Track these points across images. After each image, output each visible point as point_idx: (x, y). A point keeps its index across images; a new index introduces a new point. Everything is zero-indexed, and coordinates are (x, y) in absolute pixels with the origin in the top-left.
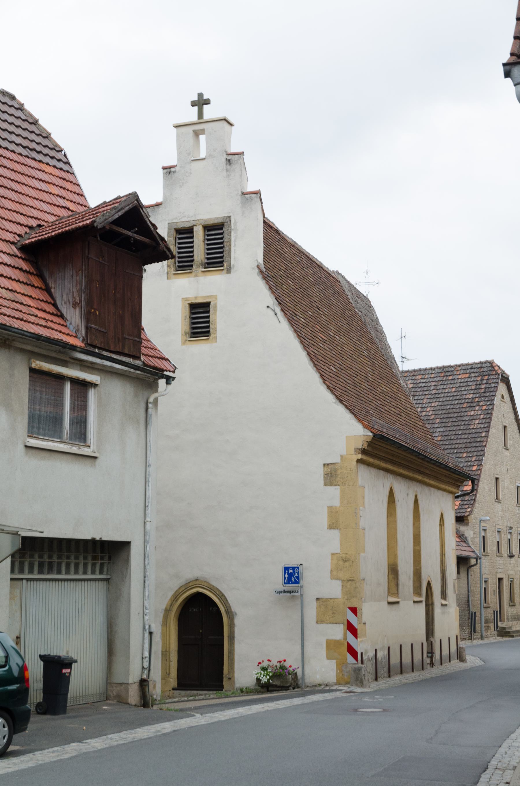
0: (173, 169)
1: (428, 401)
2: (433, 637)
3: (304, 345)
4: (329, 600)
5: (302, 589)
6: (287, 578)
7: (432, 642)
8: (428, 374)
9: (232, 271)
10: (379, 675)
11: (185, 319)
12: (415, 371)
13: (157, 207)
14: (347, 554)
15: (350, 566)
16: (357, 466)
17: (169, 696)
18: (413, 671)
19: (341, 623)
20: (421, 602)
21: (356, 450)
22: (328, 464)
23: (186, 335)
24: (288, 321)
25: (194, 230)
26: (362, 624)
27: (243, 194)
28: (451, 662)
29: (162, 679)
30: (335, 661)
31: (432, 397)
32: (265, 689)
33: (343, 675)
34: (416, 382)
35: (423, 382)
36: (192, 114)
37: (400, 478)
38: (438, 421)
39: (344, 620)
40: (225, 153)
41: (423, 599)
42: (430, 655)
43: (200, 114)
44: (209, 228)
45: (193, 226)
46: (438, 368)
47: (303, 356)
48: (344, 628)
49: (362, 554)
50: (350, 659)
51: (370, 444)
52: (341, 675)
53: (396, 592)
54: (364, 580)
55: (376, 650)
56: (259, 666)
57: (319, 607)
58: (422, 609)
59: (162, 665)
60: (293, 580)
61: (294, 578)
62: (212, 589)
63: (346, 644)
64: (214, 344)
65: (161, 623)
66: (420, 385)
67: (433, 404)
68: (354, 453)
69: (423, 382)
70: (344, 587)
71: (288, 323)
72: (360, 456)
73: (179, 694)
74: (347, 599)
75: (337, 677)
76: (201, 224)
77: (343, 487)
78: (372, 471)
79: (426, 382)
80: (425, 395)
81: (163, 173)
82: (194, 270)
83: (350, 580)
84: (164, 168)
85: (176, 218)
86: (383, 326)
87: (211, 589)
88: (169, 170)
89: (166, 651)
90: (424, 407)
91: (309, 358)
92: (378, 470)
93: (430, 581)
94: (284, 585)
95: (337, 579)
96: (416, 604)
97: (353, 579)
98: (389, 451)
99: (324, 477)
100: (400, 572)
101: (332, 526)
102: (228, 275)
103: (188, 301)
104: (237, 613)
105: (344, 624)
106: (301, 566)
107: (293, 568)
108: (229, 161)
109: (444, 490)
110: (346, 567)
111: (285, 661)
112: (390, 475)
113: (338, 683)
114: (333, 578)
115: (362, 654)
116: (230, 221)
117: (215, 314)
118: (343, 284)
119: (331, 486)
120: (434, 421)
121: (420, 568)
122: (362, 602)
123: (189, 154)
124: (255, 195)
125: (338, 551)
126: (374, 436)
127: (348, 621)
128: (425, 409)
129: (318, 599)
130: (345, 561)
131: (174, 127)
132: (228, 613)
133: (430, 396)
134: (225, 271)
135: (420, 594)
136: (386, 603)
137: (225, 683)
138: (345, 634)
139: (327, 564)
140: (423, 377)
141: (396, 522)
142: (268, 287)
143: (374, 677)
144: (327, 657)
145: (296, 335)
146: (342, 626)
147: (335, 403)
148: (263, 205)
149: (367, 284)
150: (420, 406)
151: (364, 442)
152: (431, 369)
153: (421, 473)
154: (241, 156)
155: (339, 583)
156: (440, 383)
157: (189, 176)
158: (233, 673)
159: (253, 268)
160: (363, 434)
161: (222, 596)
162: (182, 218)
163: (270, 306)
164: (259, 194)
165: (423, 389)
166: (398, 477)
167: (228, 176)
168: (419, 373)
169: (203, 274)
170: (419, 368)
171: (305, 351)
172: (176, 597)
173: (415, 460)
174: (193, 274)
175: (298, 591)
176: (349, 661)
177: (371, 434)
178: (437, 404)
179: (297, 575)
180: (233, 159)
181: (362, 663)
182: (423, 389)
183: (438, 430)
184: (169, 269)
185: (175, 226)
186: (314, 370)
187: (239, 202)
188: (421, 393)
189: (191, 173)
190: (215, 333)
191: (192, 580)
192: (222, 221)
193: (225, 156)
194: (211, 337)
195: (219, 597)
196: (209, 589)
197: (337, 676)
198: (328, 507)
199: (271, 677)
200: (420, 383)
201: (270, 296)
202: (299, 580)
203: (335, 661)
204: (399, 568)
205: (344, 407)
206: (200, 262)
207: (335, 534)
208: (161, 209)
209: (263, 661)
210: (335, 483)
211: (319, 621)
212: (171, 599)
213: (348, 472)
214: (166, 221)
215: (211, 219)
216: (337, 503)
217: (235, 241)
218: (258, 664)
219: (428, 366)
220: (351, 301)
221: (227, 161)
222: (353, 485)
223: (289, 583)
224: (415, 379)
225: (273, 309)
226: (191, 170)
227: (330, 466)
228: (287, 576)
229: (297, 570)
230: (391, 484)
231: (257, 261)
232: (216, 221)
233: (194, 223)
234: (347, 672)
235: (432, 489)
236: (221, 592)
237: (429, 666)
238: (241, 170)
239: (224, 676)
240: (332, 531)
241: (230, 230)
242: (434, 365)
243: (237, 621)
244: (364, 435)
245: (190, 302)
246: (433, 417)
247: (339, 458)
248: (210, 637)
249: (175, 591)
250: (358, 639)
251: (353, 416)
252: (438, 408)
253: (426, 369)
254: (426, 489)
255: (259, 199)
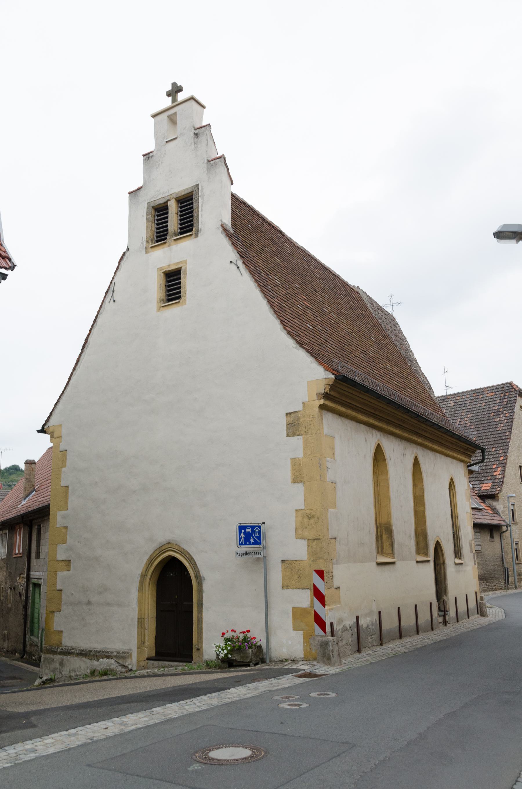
0: (151, 155)
1: (465, 413)
2: (446, 596)
3: (264, 293)
4: (295, 562)
5: (264, 550)
6: (243, 539)
7: (444, 601)
8: (465, 395)
9: (200, 234)
10: (362, 644)
11: (160, 288)
12: (455, 394)
13: (138, 191)
14: (312, 509)
15: (316, 523)
16: (321, 415)
17: (144, 666)
18: (418, 633)
19: (308, 589)
20: (428, 561)
21: (318, 395)
22: (290, 413)
23: (160, 302)
24: (249, 272)
25: (169, 204)
26: (333, 589)
27: (208, 161)
28: (470, 618)
29: (138, 648)
30: (302, 632)
31: (468, 411)
32: (226, 665)
33: (310, 649)
34: (456, 401)
35: (461, 401)
36: (168, 102)
37: (392, 438)
38: (473, 427)
39: (311, 584)
40: (193, 128)
41: (431, 558)
42: (442, 613)
43: (174, 100)
44: (181, 201)
45: (167, 202)
46: (471, 391)
47: (263, 304)
48: (310, 594)
49: (331, 510)
50: (318, 630)
51: (332, 387)
52: (308, 649)
53: (391, 552)
54: (335, 539)
55: (357, 618)
56: (223, 636)
57: (284, 570)
58: (429, 569)
59: (138, 633)
60: (252, 540)
61: (253, 538)
62: (183, 552)
63: (313, 612)
64: (184, 306)
65: (138, 588)
66: (459, 403)
67: (469, 416)
68: (316, 398)
69: (461, 401)
70: (310, 547)
71: (249, 273)
72: (322, 402)
73: (153, 665)
74: (313, 561)
75: (304, 652)
76: (174, 197)
77: (305, 436)
78: (343, 419)
79: (463, 401)
80: (463, 410)
81: (144, 160)
82: (168, 241)
83: (316, 539)
84: (144, 156)
85: (153, 197)
86: (406, 337)
87: (181, 552)
88: (148, 156)
89: (141, 618)
90: (463, 418)
91: (269, 306)
92: (358, 424)
93: (440, 541)
94: (239, 546)
95: (302, 538)
96: (420, 565)
97: (319, 537)
98: (364, 401)
99: (287, 427)
100: (395, 532)
101: (295, 481)
102: (196, 239)
103: (163, 270)
104: (205, 578)
105: (310, 590)
106: (263, 525)
107: (253, 527)
108: (196, 135)
109: (453, 458)
110: (311, 525)
111: (248, 631)
112: (376, 431)
113: (306, 659)
114: (299, 537)
115: (332, 624)
116: (198, 188)
117: (185, 278)
118: (362, 296)
119: (294, 436)
120: (470, 427)
121: (426, 528)
122: (333, 564)
123: (164, 137)
124: (219, 160)
125: (303, 507)
126: (336, 378)
127: (315, 586)
128: (463, 420)
129: (283, 561)
130: (310, 517)
131: (231, 194)
132: (197, 578)
133: (466, 410)
134: (194, 236)
135: (426, 554)
136: (415, 562)
137: (195, 654)
138: (312, 601)
139: (292, 522)
140: (461, 397)
141: (388, 480)
142: (230, 243)
143: (356, 649)
144: (293, 627)
145: (257, 285)
146: (308, 591)
147: (295, 348)
148: (229, 171)
149: (392, 305)
150: (460, 417)
151: (326, 385)
152: (467, 392)
153: (420, 436)
154: (208, 128)
155: (304, 543)
156: (474, 400)
157: (164, 157)
158: (202, 643)
159: (218, 228)
160: (325, 377)
161: (191, 560)
162: (158, 196)
163: (233, 261)
164: (222, 159)
165: (461, 406)
166: (389, 436)
167: (196, 148)
168: (458, 395)
169: (175, 242)
170: (458, 392)
171: (266, 299)
172: (150, 562)
173: (408, 420)
174: (167, 244)
175: (260, 553)
176: (316, 633)
177: (333, 377)
178: (471, 415)
179: (257, 535)
180: (200, 132)
181: (333, 635)
182: (461, 406)
183: (474, 433)
184: (147, 244)
185: (152, 205)
186: (274, 317)
187: (205, 169)
188: (460, 409)
189: (165, 154)
190: (185, 295)
191: (165, 544)
192: (192, 190)
193: (193, 131)
194: (181, 301)
195: (189, 561)
196: (180, 552)
197: (304, 650)
198: (291, 459)
199: (230, 652)
200: (459, 402)
201: (233, 251)
202: (260, 540)
203: (302, 632)
204: (394, 528)
205: (304, 351)
206: (173, 232)
207: (300, 487)
208: (142, 192)
209: (228, 631)
210: (298, 433)
211: (285, 587)
212: (146, 563)
213: (311, 419)
214: (146, 201)
215: (181, 191)
216: (300, 454)
217: (202, 206)
218: (221, 635)
219: (465, 390)
220: (372, 311)
221: (195, 135)
222: (316, 434)
223: (245, 544)
224: (455, 400)
225: (236, 263)
226: (166, 151)
227: (292, 415)
228: (242, 535)
229: (257, 529)
230: (378, 440)
231: (221, 220)
232: (186, 192)
233: (168, 198)
234: (315, 646)
235: (438, 455)
236: (191, 556)
237: (441, 624)
238: (207, 140)
239: (193, 646)
240: (296, 485)
241: (198, 198)
242: (469, 389)
243: (206, 587)
244: (326, 378)
245: (164, 271)
246: (469, 424)
247: (301, 405)
248: (185, 603)
249: (150, 555)
250: (326, 607)
251: (314, 359)
252: (473, 418)
253: (463, 392)
254: (430, 454)
255: (224, 164)
